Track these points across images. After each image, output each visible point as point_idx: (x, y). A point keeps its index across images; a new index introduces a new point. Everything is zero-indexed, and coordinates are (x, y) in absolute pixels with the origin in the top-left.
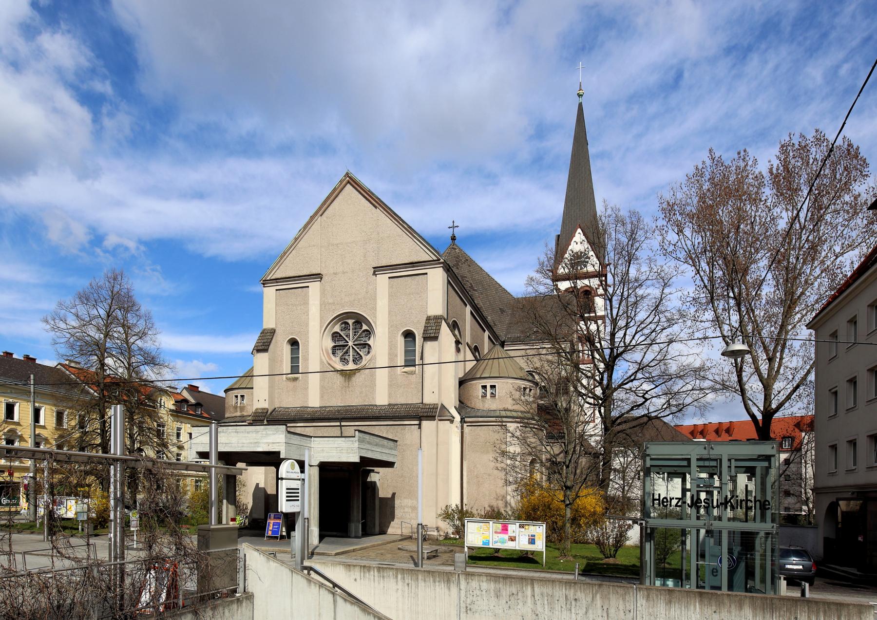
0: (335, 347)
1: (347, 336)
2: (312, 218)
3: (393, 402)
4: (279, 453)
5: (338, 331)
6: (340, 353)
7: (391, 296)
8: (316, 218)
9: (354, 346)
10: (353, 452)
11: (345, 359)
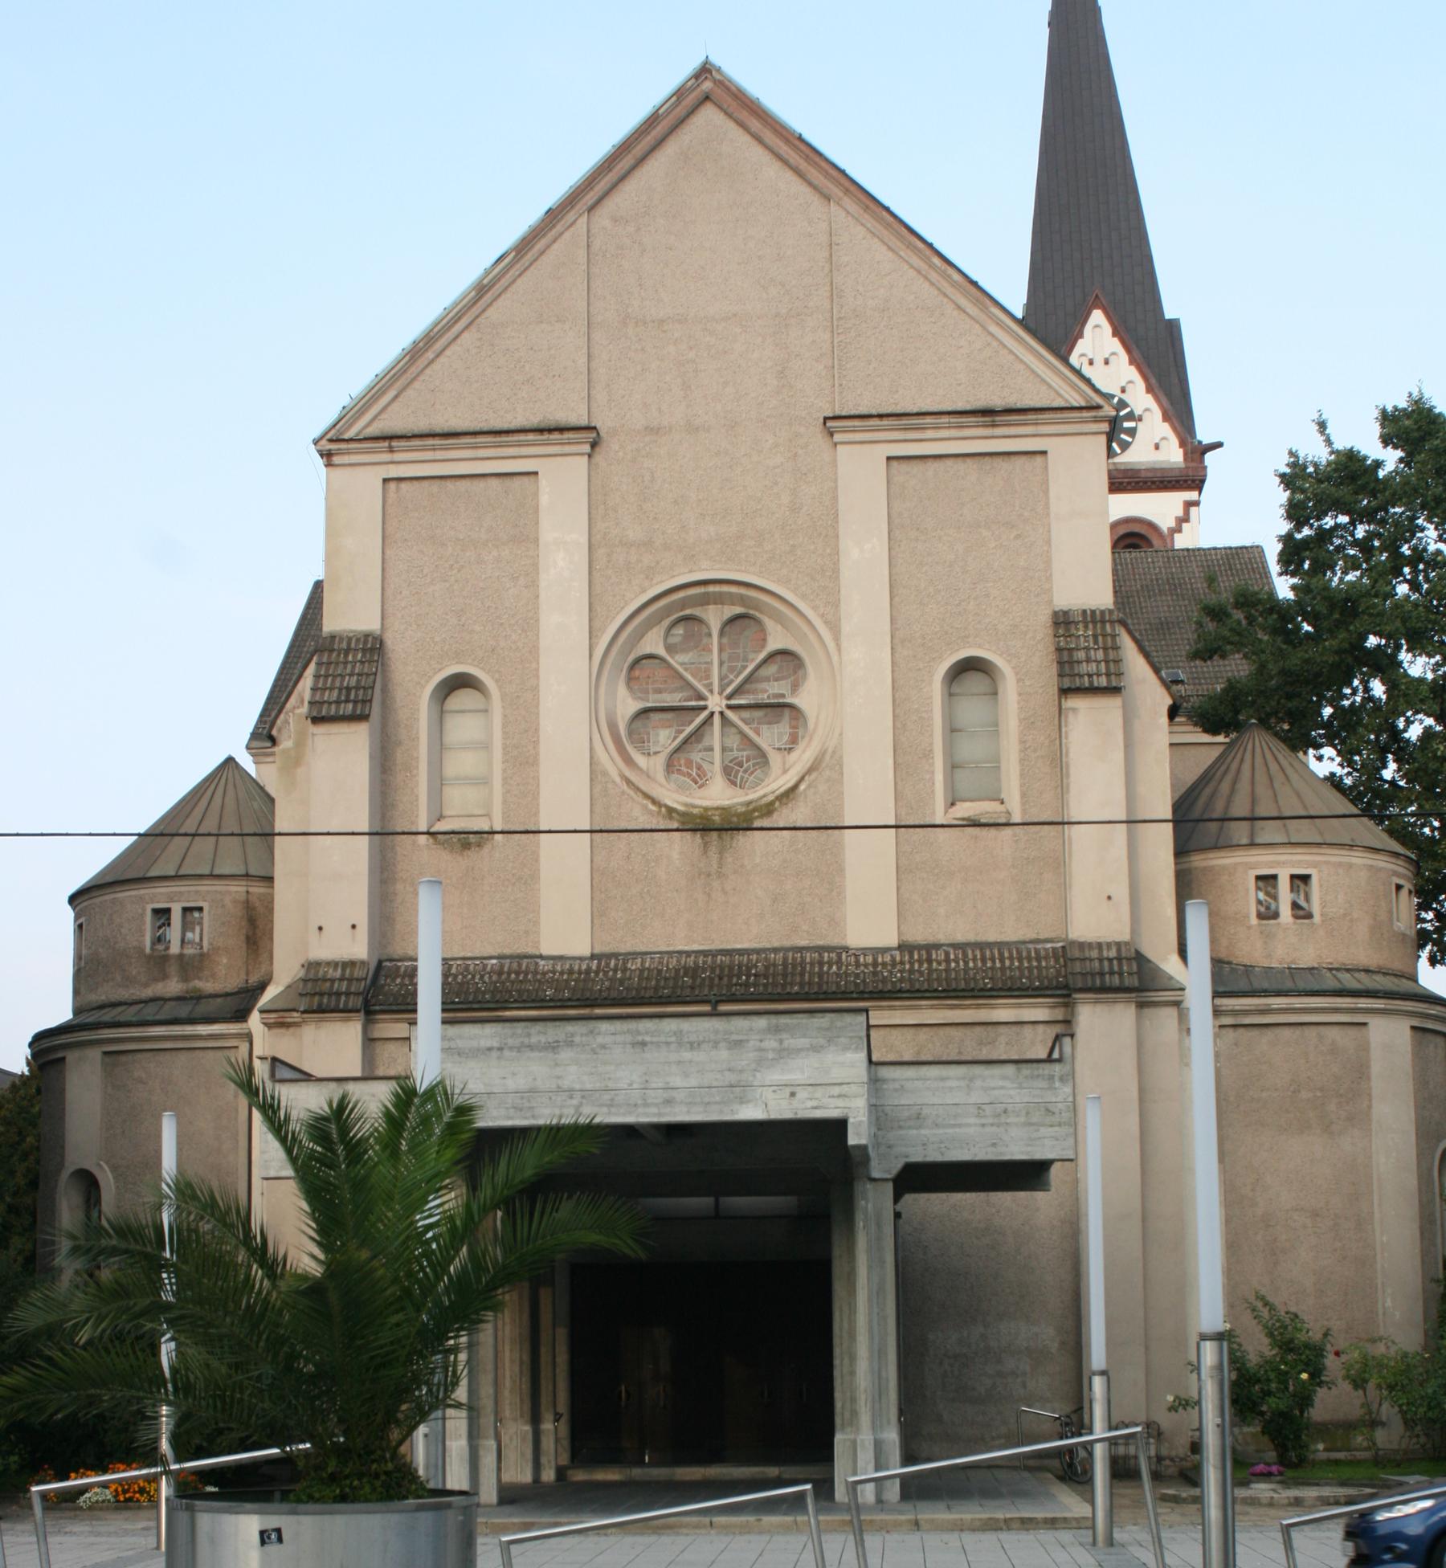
0: (645, 712)
2: (553, 216)
3: (919, 934)
4: (839, 1126)
5: (661, 651)
6: (665, 737)
8: (571, 217)
10: (1056, 1119)
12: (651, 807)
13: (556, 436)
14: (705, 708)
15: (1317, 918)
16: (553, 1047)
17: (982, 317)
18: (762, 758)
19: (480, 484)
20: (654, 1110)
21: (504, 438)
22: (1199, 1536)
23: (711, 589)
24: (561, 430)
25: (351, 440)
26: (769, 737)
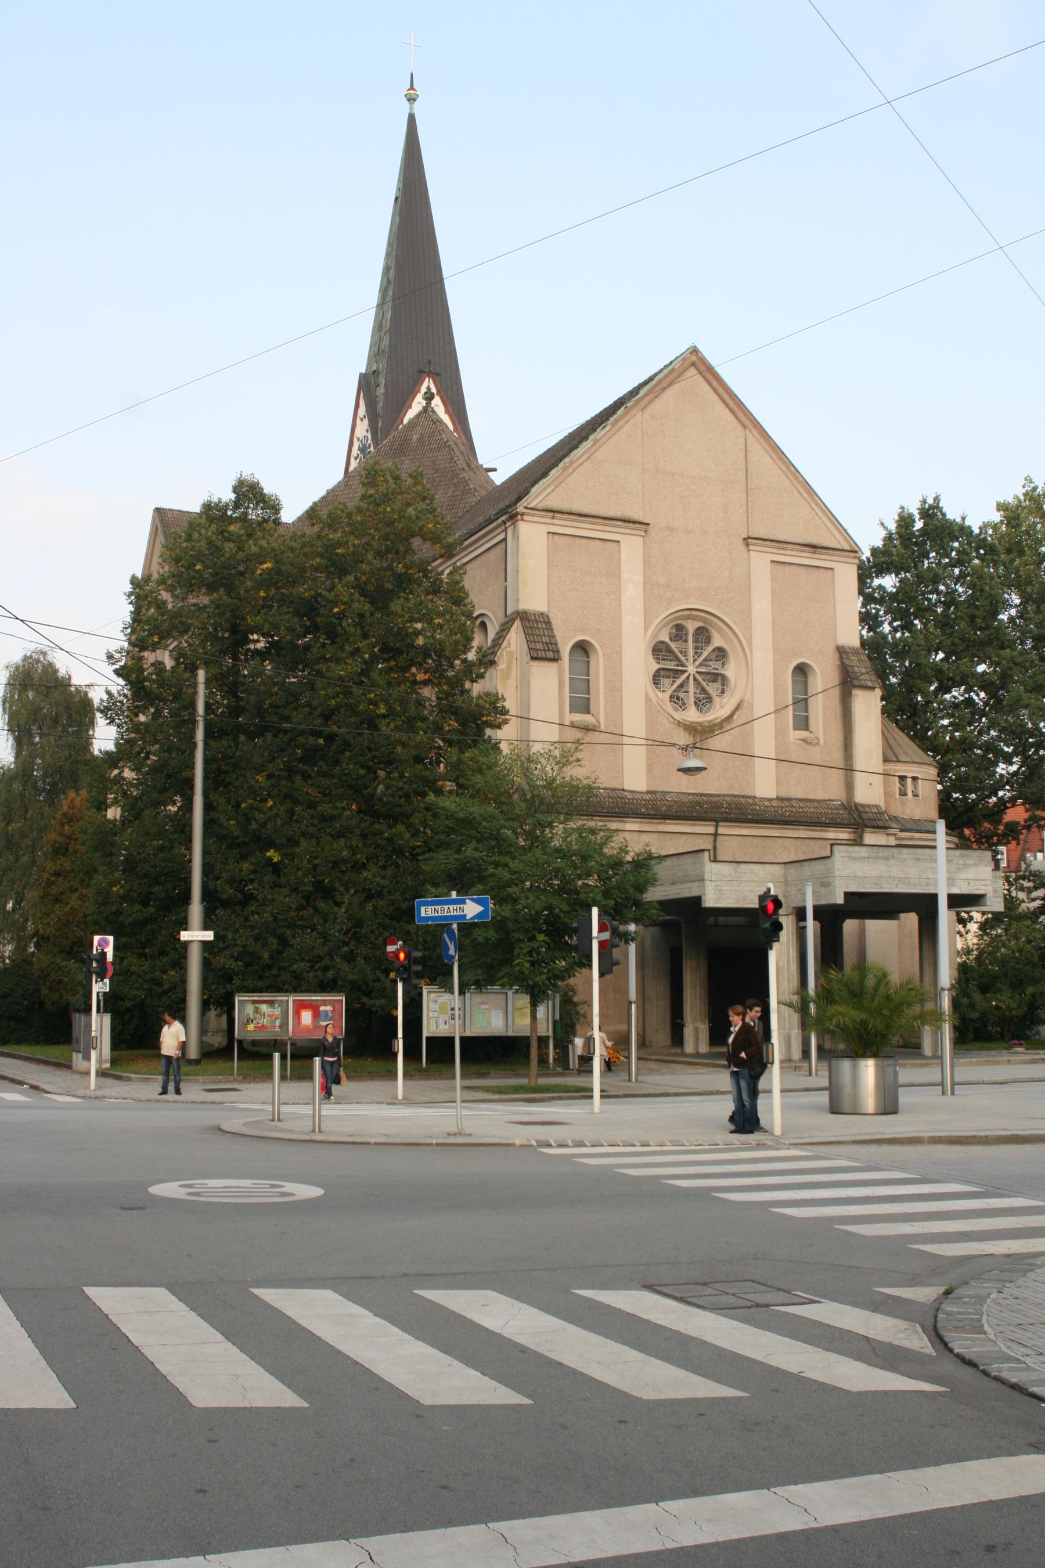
0: (659, 670)
1: (681, 652)
3: (784, 794)
5: (667, 640)
7: (776, 596)
9: (698, 677)
11: (678, 698)
12: (672, 720)
13: (631, 525)
14: (685, 671)
15: (920, 797)
16: (887, 858)
17: (810, 500)
18: (709, 699)
19: (592, 543)
20: (922, 887)
21: (607, 522)
22: (827, 1073)
23: (693, 613)
24: (634, 522)
25: (532, 509)
26: (712, 689)
